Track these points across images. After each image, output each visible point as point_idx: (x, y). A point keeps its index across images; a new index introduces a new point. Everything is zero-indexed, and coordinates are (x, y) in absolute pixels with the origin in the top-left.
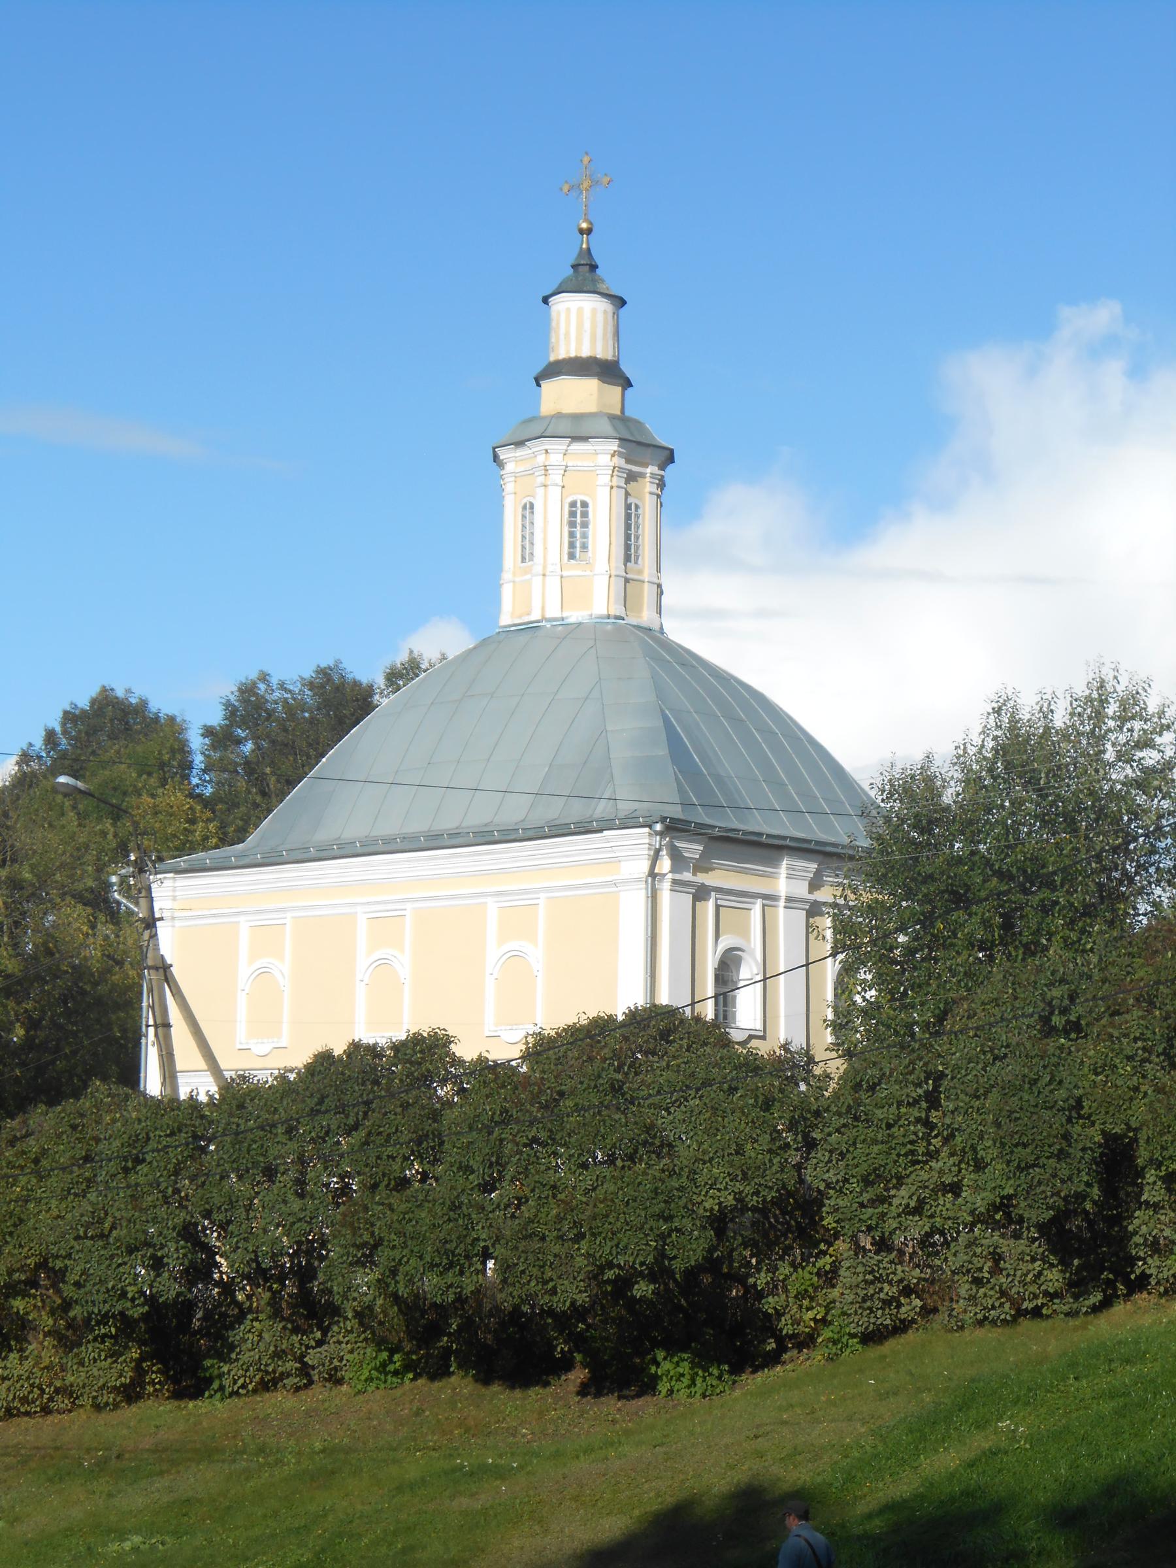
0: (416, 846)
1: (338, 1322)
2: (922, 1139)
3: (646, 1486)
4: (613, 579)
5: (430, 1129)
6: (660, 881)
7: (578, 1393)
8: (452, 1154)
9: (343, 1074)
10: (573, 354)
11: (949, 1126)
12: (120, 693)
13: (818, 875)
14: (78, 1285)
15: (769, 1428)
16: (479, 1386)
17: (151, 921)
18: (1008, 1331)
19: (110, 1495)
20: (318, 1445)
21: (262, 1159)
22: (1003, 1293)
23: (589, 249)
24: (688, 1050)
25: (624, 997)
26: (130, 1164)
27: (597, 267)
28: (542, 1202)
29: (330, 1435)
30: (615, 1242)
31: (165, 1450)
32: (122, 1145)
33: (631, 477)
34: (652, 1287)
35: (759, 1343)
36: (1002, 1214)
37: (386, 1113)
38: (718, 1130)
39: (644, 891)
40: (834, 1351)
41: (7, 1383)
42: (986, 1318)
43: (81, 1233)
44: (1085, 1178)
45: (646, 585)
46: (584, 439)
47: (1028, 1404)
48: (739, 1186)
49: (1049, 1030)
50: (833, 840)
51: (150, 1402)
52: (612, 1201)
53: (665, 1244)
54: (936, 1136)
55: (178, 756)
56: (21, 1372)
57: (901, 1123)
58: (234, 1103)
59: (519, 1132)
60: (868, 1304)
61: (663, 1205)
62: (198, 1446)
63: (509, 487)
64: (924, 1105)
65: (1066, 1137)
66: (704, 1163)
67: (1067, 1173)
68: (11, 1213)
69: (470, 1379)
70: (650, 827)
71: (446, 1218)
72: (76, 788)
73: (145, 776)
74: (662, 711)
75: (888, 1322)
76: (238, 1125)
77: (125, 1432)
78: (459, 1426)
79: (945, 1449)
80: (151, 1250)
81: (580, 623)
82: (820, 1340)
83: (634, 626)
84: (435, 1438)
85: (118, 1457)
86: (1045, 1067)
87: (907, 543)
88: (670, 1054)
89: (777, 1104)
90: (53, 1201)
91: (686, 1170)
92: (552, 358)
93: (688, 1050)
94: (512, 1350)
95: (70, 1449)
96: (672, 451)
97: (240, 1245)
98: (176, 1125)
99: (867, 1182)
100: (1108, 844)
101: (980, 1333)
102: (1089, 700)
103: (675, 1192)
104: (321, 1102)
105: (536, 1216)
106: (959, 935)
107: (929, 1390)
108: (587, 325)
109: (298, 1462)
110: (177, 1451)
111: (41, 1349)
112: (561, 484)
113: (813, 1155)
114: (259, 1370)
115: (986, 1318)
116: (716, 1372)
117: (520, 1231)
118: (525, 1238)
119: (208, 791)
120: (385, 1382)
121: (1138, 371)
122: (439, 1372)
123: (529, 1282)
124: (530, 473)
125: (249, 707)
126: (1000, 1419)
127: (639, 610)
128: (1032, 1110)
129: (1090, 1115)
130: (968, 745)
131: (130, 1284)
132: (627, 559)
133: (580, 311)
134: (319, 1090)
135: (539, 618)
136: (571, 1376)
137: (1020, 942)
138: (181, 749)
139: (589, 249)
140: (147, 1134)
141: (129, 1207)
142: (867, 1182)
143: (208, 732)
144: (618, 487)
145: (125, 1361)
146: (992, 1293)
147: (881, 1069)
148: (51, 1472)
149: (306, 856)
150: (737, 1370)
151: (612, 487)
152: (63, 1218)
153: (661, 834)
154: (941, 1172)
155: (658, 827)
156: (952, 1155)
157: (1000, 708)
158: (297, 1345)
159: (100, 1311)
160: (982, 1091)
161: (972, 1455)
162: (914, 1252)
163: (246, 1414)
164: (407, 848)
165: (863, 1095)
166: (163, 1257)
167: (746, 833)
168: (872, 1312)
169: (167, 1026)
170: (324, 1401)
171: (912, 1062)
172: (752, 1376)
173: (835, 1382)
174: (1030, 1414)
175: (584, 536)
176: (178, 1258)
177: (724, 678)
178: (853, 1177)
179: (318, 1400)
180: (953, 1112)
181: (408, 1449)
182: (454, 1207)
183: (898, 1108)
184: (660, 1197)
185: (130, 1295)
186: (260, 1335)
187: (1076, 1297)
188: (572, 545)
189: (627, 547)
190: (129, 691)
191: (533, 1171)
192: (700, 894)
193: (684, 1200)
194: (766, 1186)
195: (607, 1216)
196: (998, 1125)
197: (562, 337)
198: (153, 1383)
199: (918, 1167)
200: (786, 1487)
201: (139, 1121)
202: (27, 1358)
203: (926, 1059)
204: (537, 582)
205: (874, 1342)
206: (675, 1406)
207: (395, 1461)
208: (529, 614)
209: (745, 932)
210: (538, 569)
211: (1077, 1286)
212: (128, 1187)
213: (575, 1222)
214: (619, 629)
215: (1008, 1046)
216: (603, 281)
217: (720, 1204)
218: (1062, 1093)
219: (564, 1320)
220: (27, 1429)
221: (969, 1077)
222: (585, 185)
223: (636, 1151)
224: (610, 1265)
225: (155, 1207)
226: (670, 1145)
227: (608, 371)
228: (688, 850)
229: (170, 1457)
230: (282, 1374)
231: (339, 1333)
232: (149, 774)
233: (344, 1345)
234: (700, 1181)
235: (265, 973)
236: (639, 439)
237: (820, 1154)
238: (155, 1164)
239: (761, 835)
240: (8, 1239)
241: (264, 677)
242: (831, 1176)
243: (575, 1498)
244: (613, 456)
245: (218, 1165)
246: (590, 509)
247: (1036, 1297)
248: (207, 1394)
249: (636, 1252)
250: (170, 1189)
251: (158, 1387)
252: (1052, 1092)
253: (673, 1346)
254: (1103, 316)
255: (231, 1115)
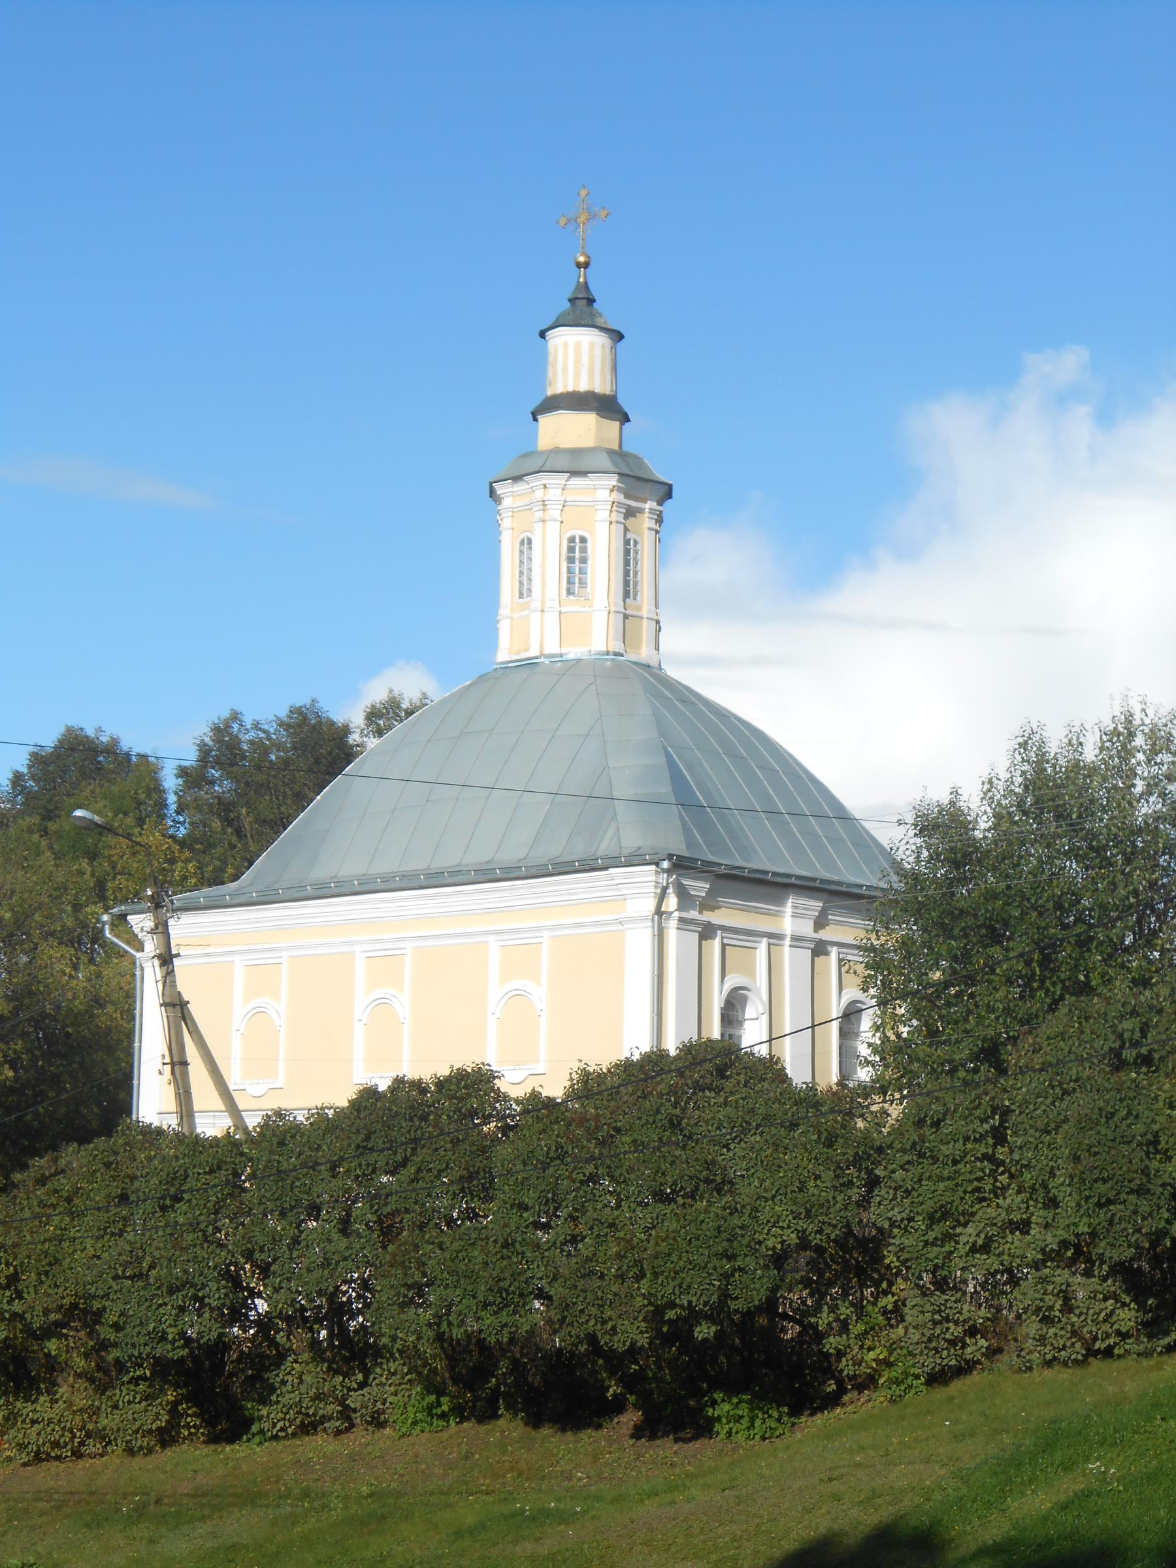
0: (417, 885)
1: (381, 1364)
2: (989, 1176)
3: (720, 1531)
4: (612, 615)
5: (482, 1165)
6: (667, 919)
7: (632, 1436)
8: (505, 1192)
9: (390, 1110)
10: (570, 389)
11: (1018, 1162)
12: (90, 732)
13: (823, 913)
14: (117, 1327)
15: (843, 1471)
16: (529, 1429)
17: (167, 957)
18: (1079, 1372)
19: (152, 1541)
20: (365, 1490)
21: (305, 1197)
22: (1074, 1333)
23: (586, 283)
24: (745, 1086)
25: (633, 1041)
26: (168, 1202)
27: (594, 301)
28: (600, 1240)
29: (376, 1479)
30: (677, 1282)
31: (204, 1495)
32: (161, 1182)
33: (630, 513)
34: (713, 1328)
35: (820, 1384)
36: (1077, 1253)
37: (436, 1150)
38: (780, 1167)
39: (650, 931)
40: (898, 1393)
41: (37, 1427)
42: (1055, 1358)
43: (120, 1273)
44: (1166, 1215)
45: (645, 622)
46: (583, 473)
47: (1115, 1444)
48: (802, 1224)
49: (1119, 1064)
50: (836, 878)
51: (184, 1447)
52: (675, 1239)
53: (728, 1284)
54: (1002, 1173)
55: (154, 796)
56: (51, 1415)
57: (967, 1159)
58: (275, 1140)
59: (575, 1168)
60: (934, 1344)
61: (725, 1244)
62: (240, 1490)
63: (506, 522)
64: (991, 1141)
65: (1145, 1172)
66: (766, 1201)
67: (1148, 1209)
68: (46, 1252)
69: (519, 1421)
70: (657, 864)
71: (499, 1256)
72: (92, 821)
73: (121, 816)
74: (664, 748)
75: (953, 1362)
76: (279, 1162)
77: (162, 1476)
78: (511, 1470)
79: (1033, 1491)
80: (192, 1290)
81: (579, 660)
82: (881, 1381)
83: (634, 663)
84: (488, 1481)
85: (157, 1502)
86: (1121, 1100)
87: (870, 591)
88: (727, 1090)
89: (840, 1140)
90: (88, 1240)
91: (749, 1207)
92: (549, 393)
93: (745, 1086)
94: (562, 1391)
95: (106, 1494)
96: (670, 487)
97: (283, 1285)
98: (215, 1162)
99: (932, 1220)
100: (1144, 878)
101: (1048, 1373)
102: (1115, 732)
103: (738, 1231)
104: (368, 1138)
105: (594, 1255)
106: (998, 971)
107: (1007, 1432)
108: (585, 359)
109: (346, 1507)
110: (218, 1495)
111: (72, 1393)
112: (559, 519)
113: (876, 1192)
114: (299, 1413)
115: (1055, 1358)
116: (775, 1414)
117: (578, 1270)
118: (583, 1276)
119: (182, 832)
120: (432, 1424)
121: (1105, 418)
122: (487, 1414)
123: (587, 1321)
124: (528, 508)
125: (224, 749)
126: (1087, 1459)
127: (638, 646)
128: (1111, 1144)
129: (1167, 1150)
130: (994, 780)
131: (170, 1326)
132: (626, 594)
133: (578, 345)
134: (365, 1127)
135: (537, 654)
136: (624, 1418)
137: (1058, 977)
138: (157, 790)
139: (586, 283)
140: (185, 1171)
141: (169, 1246)
142: (932, 1220)
143: (183, 772)
144: (618, 522)
145: (161, 1404)
146: (1063, 1333)
147: (945, 1105)
148: (88, 1518)
149: (302, 894)
150: (796, 1412)
151: (611, 523)
152: (98, 1258)
153: (669, 872)
154: (1009, 1210)
155: (665, 864)
156: (1019, 1192)
157: (1026, 743)
158: (339, 1387)
159: (140, 1354)
160: (1053, 1125)
161: (1063, 1497)
162: (976, 1292)
163: (287, 1458)
164: (404, 886)
165: (927, 1131)
166: (204, 1297)
167: (752, 871)
168: (937, 1352)
169: (184, 1064)
170: (367, 1445)
171: (979, 1097)
172: (811, 1419)
173: (905, 1423)
174: (1118, 1455)
175: (582, 572)
176: (219, 1298)
177: (724, 715)
178: (918, 1214)
179: (360, 1444)
180: (1021, 1148)
181: (460, 1493)
182: (506, 1245)
183: (964, 1145)
184: (724, 1236)
185: (170, 1337)
186: (300, 1378)
187: (1150, 1337)
188: (570, 582)
189: (626, 583)
190: (100, 730)
191: (590, 1208)
192: (707, 932)
193: (747, 1238)
194: (830, 1224)
195: (669, 1255)
196: (1077, 1159)
197: (559, 371)
198: (188, 1426)
199: (985, 1204)
200: (862, 1531)
201: (177, 1158)
202: (57, 1401)
203: (993, 1094)
204: (535, 617)
205: (940, 1383)
206: (734, 1449)
207: (447, 1506)
208: (527, 650)
209: (751, 972)
210: (537, 604)
211: (1152, 1327)
212: (167, 1225)
213: (635, 1261)
214: (618, 666)
215: (1076, 1081)
216: (601, 315)
217: (783, 1242)
218: (1139, 1128)
219: (616, 1361)
220: (58, 1474)
221: (1038, 1112)
222: (583, 218)
223: (697, 1188)
224: (672, 1305)
225: (195, 1246)
226: (731, 1182)
227: (606, 406)
228: (695, 888)
229: (210, 1502)
230: (323, 1416)
231: (381, 1375)
232: (126, 814)
233: (387, 1388)
234: (763, 1218)
235: (266, 1014)
236: (639, 474)
237: (882, 1192)
238: (194, 1201)
239: (767, 872)
240: (43, 1278)
241: (235, 716)
242: (896, 1214)
243: (646, 1543)
244: (612, 491)
245: (260, 1204)
246: (589, 545)
247: (1108, 1336)
248: (245, 1438)
249: (699, 1292)
250: (211, 1227)
251: (193, 1430)
252: (1129, 1126)
253: (733, 1388)
254: (1069, 364)
255: (272, 1152)
